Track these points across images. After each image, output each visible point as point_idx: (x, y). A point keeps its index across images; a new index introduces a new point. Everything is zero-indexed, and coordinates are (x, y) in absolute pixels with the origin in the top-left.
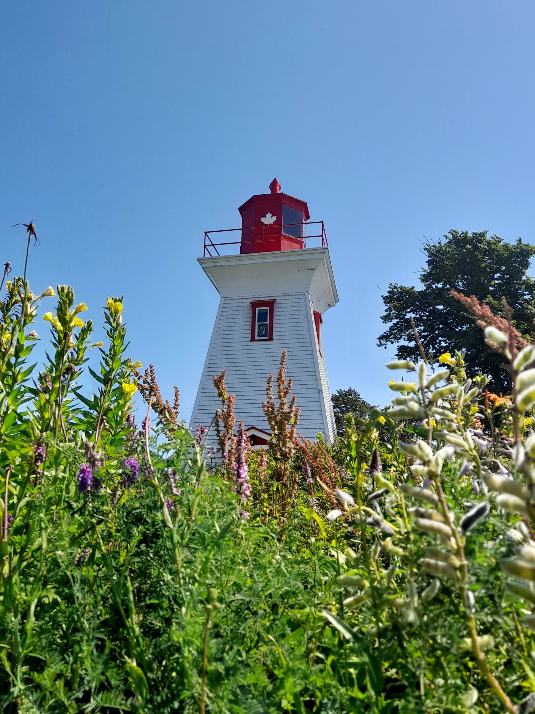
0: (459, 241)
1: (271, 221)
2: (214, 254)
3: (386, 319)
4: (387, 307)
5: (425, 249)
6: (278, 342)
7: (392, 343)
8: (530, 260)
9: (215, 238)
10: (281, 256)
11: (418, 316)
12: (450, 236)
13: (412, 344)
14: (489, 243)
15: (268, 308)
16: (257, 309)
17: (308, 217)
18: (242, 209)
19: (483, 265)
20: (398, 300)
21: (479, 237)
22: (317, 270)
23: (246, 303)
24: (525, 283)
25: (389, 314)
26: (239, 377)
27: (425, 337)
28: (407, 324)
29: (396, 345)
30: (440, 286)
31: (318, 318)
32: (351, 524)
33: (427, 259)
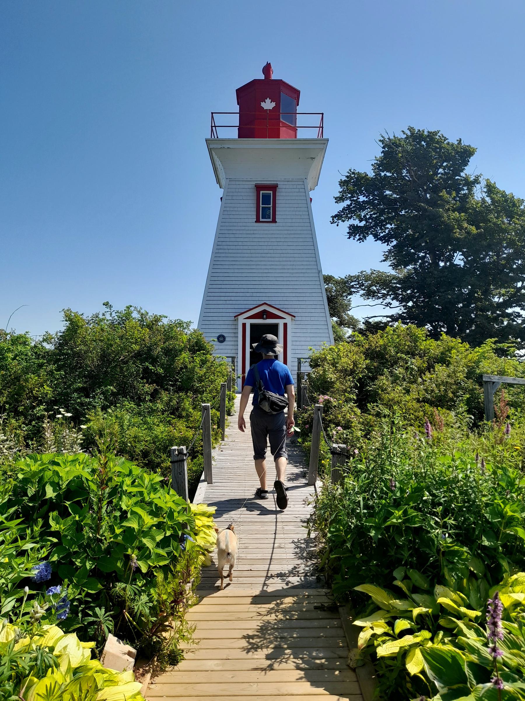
0: (416, 137)
1: (265, 108)
3: (339, 200)
4: (342, 189)
5: (380, 141)
6: (281, 224)
12: (409, 134)
15: (271, 192)
16: (261, 192)
21: (431, 136)
26: (247, 255)
28: (361, 206)
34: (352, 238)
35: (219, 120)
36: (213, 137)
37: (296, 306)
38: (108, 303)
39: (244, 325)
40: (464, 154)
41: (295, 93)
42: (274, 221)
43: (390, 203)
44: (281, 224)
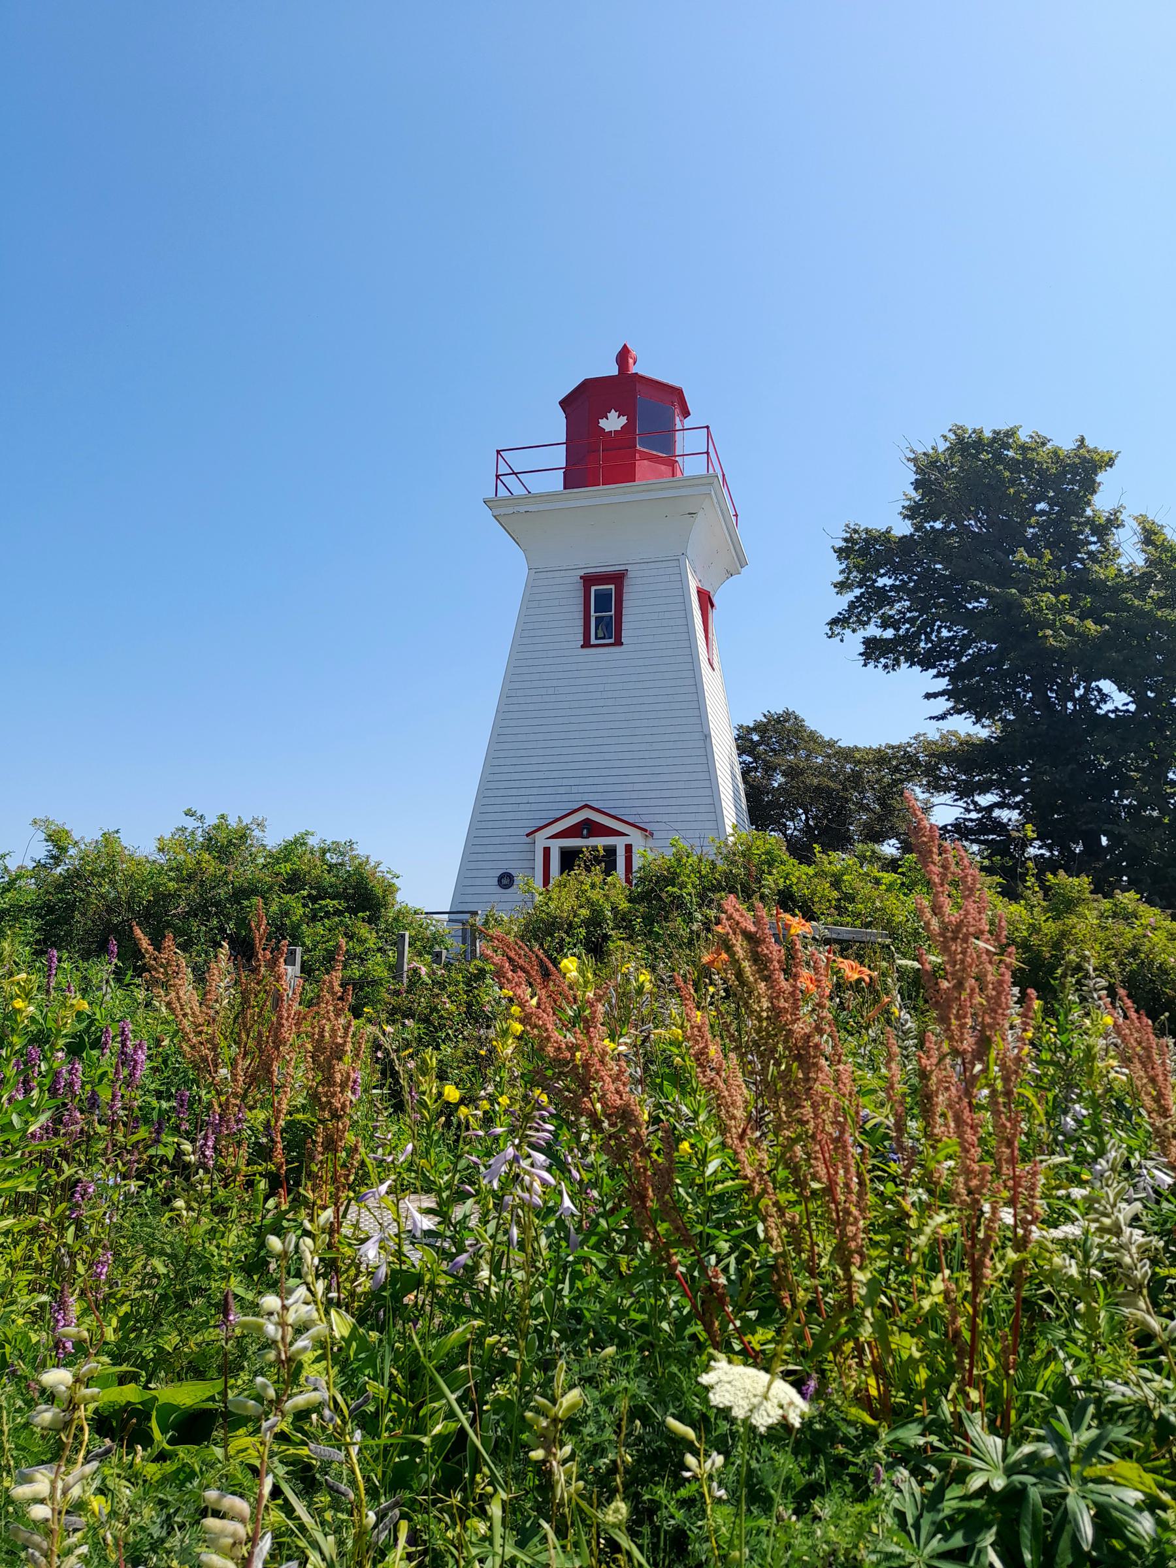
0: (967, 446)
1: (619, 425)
2: (518, 490)
3: (842, 587)
4: (844, 566)
7: (854, 631)
8: (1098, 479)
9: (518, 461)
11: (898, 583)
13: (889, 633)
14: (1023, 448)
16: (593, 589)
17: (686, 413)
18: (565, 404)
19: (1012, 490)
20: (863, 553)
21: (1002, 439)
22: (701, 514)
23: (573, 582)
24: (1090, 522)
25: (848, 578)
27: (912, 621)
28: (881, 597)
29: (863, 633)
30: (938, 525)
31: (706, 600)
33: (913, 477)
34: (871, 665)
36: (711, 471)
37: (656, 810)
39: (547, 851)
40: (1085, 468)
41: (689, 414)
43: (941, 586)
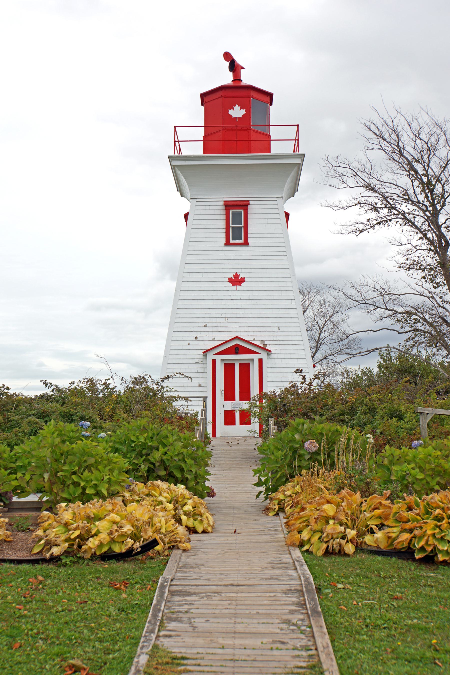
10: (242, 638)
32: (343, 421)
35: (182, 134)
38: (236, 276)
39: (214, 362)
41: (270, 96)
42: (246, 243)
44: (253, 249)
